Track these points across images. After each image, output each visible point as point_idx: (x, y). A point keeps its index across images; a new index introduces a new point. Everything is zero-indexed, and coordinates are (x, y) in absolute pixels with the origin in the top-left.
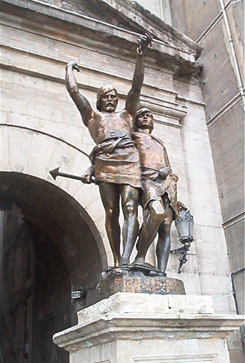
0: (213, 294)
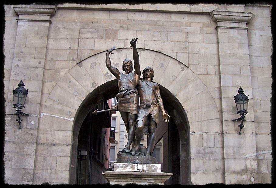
0: (268, 148)
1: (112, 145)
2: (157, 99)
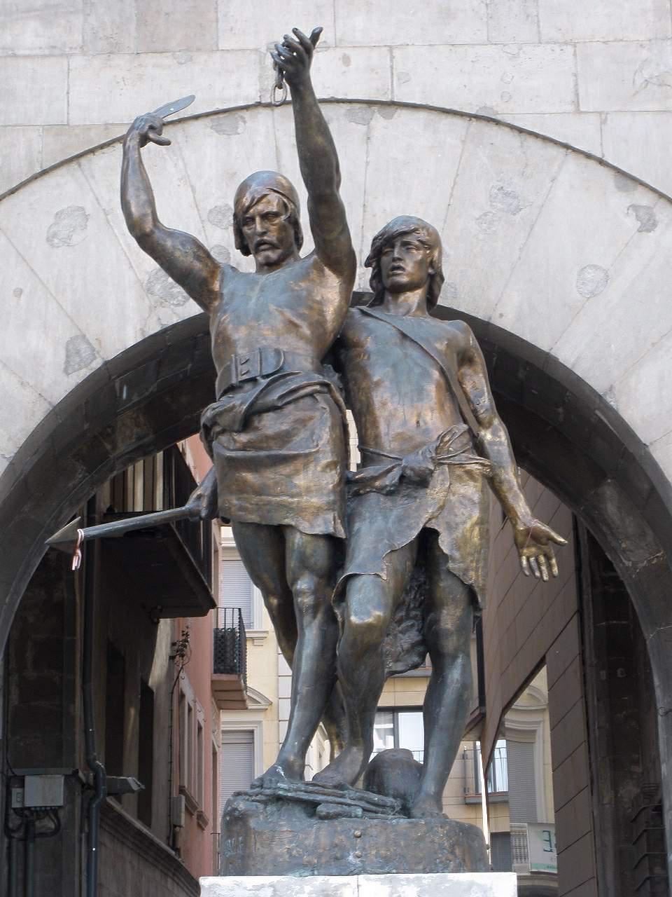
1: (230, 719)
2: (470, 431)
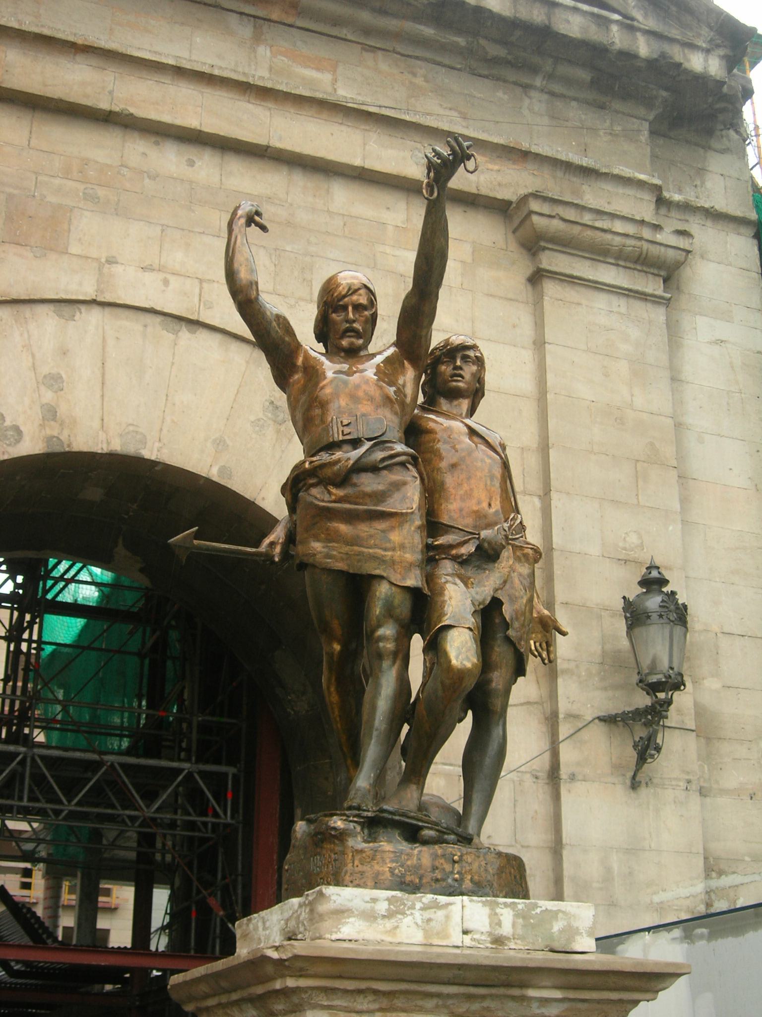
0: (747, 859)
